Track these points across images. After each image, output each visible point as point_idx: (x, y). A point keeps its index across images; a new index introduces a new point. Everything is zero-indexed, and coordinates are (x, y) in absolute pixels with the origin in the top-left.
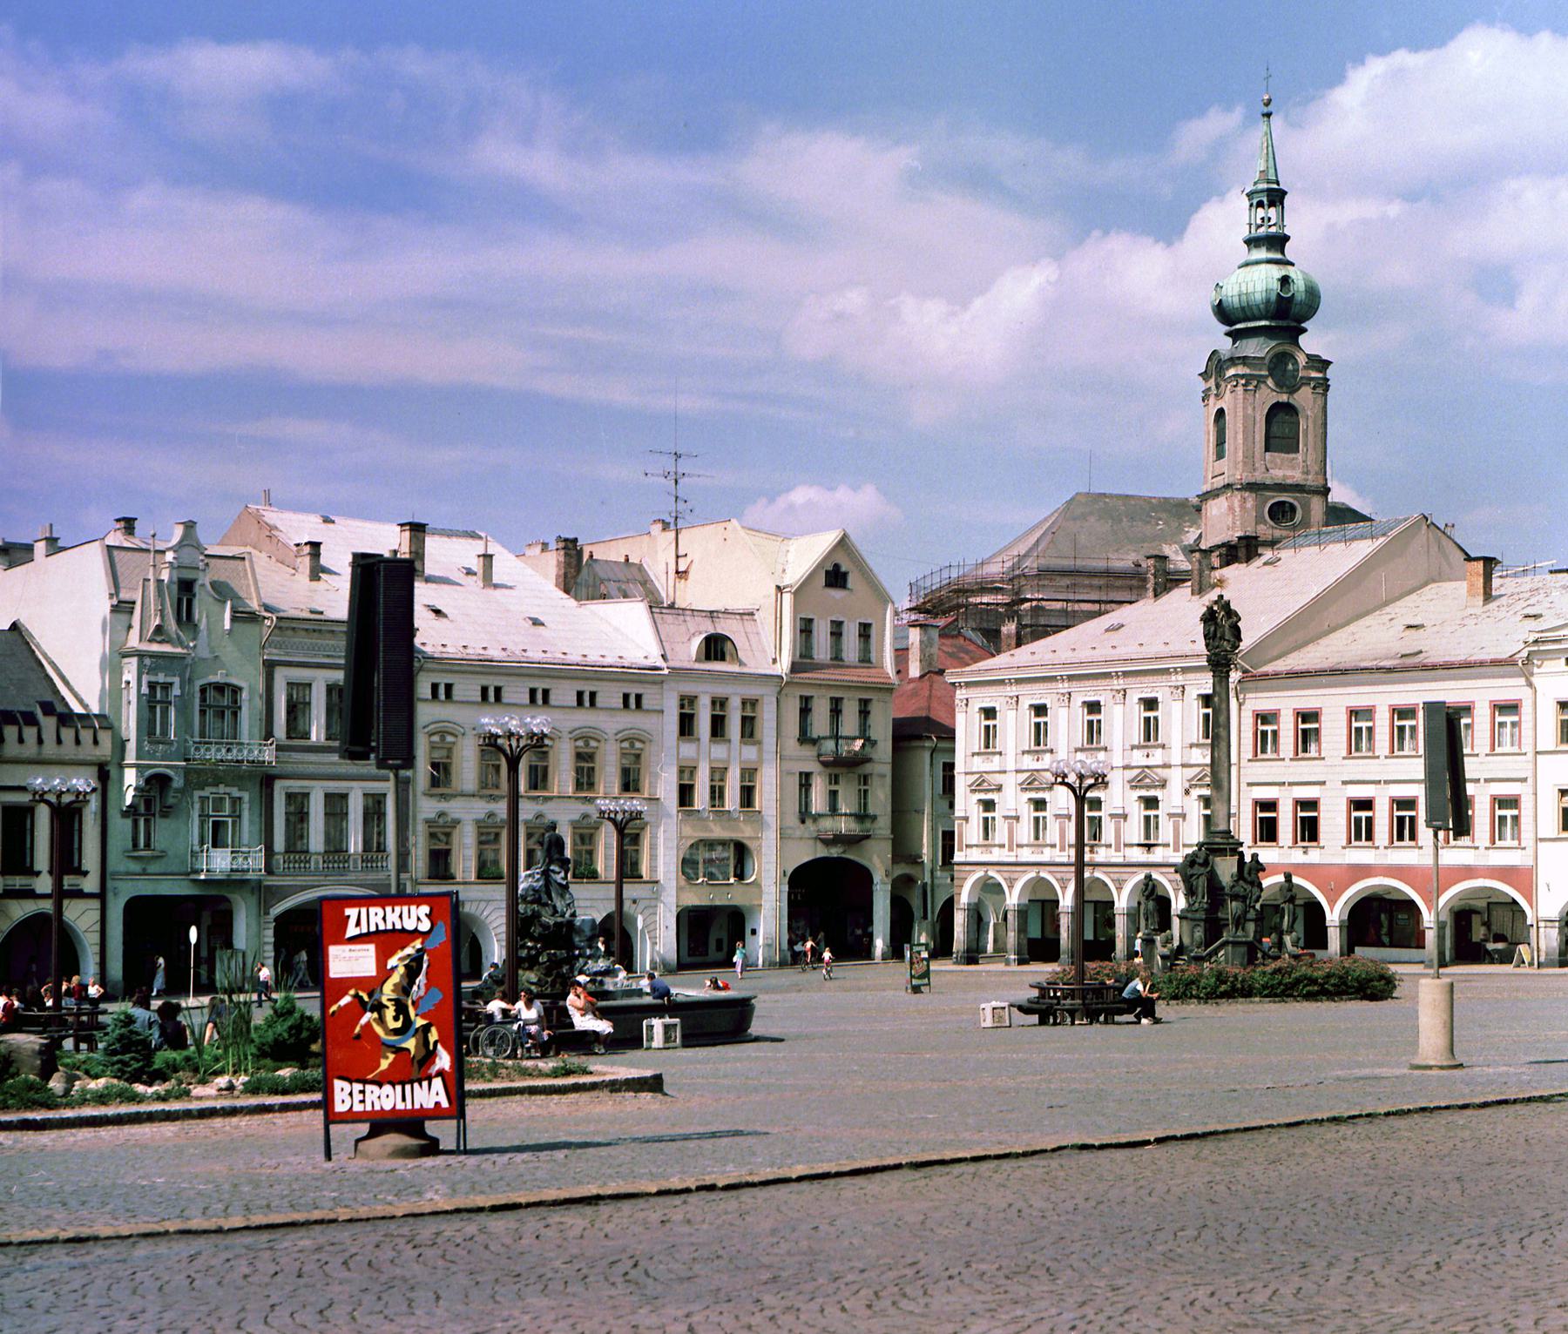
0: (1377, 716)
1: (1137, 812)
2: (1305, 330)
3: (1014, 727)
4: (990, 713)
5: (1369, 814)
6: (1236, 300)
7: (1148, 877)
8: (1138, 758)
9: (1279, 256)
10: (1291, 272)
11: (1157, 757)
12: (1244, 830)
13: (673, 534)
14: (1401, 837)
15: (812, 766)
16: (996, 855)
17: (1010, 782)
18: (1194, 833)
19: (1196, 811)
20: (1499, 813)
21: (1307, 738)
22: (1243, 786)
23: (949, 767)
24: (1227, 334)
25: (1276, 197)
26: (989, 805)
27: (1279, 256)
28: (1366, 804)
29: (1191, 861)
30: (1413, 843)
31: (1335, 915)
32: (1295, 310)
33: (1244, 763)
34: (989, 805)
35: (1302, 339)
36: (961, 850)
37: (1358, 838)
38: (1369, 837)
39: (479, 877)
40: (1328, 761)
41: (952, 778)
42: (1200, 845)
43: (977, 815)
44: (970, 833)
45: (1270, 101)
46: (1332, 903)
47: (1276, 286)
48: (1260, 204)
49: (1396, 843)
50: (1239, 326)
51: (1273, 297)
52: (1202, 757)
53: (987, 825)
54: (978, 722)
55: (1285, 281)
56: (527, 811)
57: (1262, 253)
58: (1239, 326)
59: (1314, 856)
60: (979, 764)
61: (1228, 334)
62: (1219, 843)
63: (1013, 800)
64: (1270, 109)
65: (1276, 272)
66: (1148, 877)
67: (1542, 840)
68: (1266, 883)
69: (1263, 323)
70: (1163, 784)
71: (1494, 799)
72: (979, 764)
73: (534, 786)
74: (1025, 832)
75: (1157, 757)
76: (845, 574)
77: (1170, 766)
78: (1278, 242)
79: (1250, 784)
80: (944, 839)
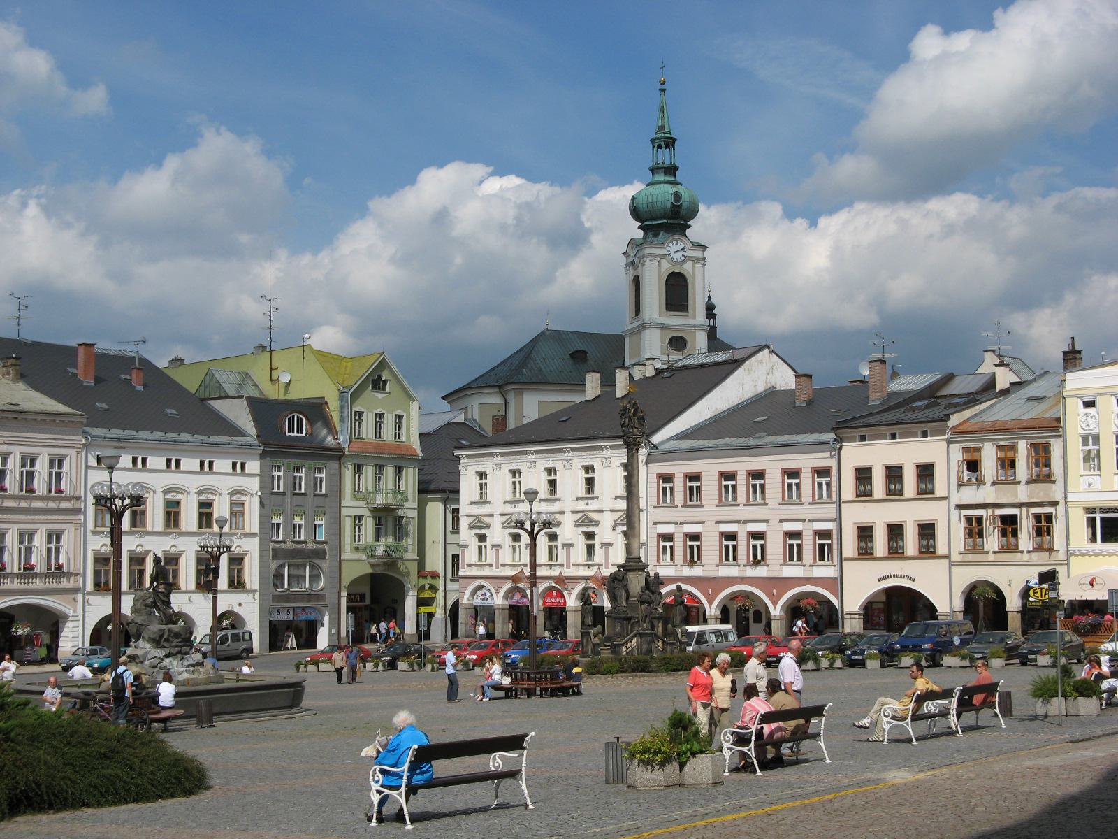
0: (803, 475)
1: (581, 543)
2: (690, 226)
3: (499, 486)
4: (482, 475)
5: (175, 567)
6: (645, 206)
7: (679, 588)
8: (581, 506)
9: (672, 179)
10: (680, 189)
11: (594, 505)
12: (648, 555)
13: (269, 354)
14: (822, 558)
15: (365, 512)
16: (487, 572)
17: (497, 522)
18: (619, 556)
19: (620, 542)
20: (789, 542)
21: (694, 493)
22: (650, 524)
23: (456, 511)
24: (640, 227)
25: (670, 143)
26: (482, 538)
27: (672, 179)
28: (732, 537)
29: (614, 578)
30: (799, 563)
31: (776, 611)
32: (683, 212)
33: (651, 509)
34: (482, 538)
35: (688, 231)
36: (463, 568)
37: (791, 558)
38: (800, 558)
39: (230, 586)
40: (769, 507)
41: (458, 519)
42: (620, 567)
43: (474, 543)
44: (471, 556)
45: (664, 82)
46: (710, 603)
47: (671, 198)
48: (660, 147)
49: (819, 563)
50: (647, 223)
51: (669, 205)
52: (622, 505)
53: (590, 549)
54: (476, 481)
55: (677, 195)
56: (129, 544)
57: (660, 177)
58: (647, 223)
59: (761, 572)
60: (476, 510)
61: (640, 227)
62: (633, 563)
63: (497, 534)
64: (664, 87)
65: (670, 189)
66: (679, 588)
67: (847, 559)
68: (664, 591)
69: (665, 221)
70: (597, 524)
71: (722, 534)
72: (476, 510)
73: (134, 524)
74: (579, 554)
75: (594, 505)
76: (385, 382)
77: (601, 511)
78: (671, 170)
79: (655, 524)
80: (453, 559)
